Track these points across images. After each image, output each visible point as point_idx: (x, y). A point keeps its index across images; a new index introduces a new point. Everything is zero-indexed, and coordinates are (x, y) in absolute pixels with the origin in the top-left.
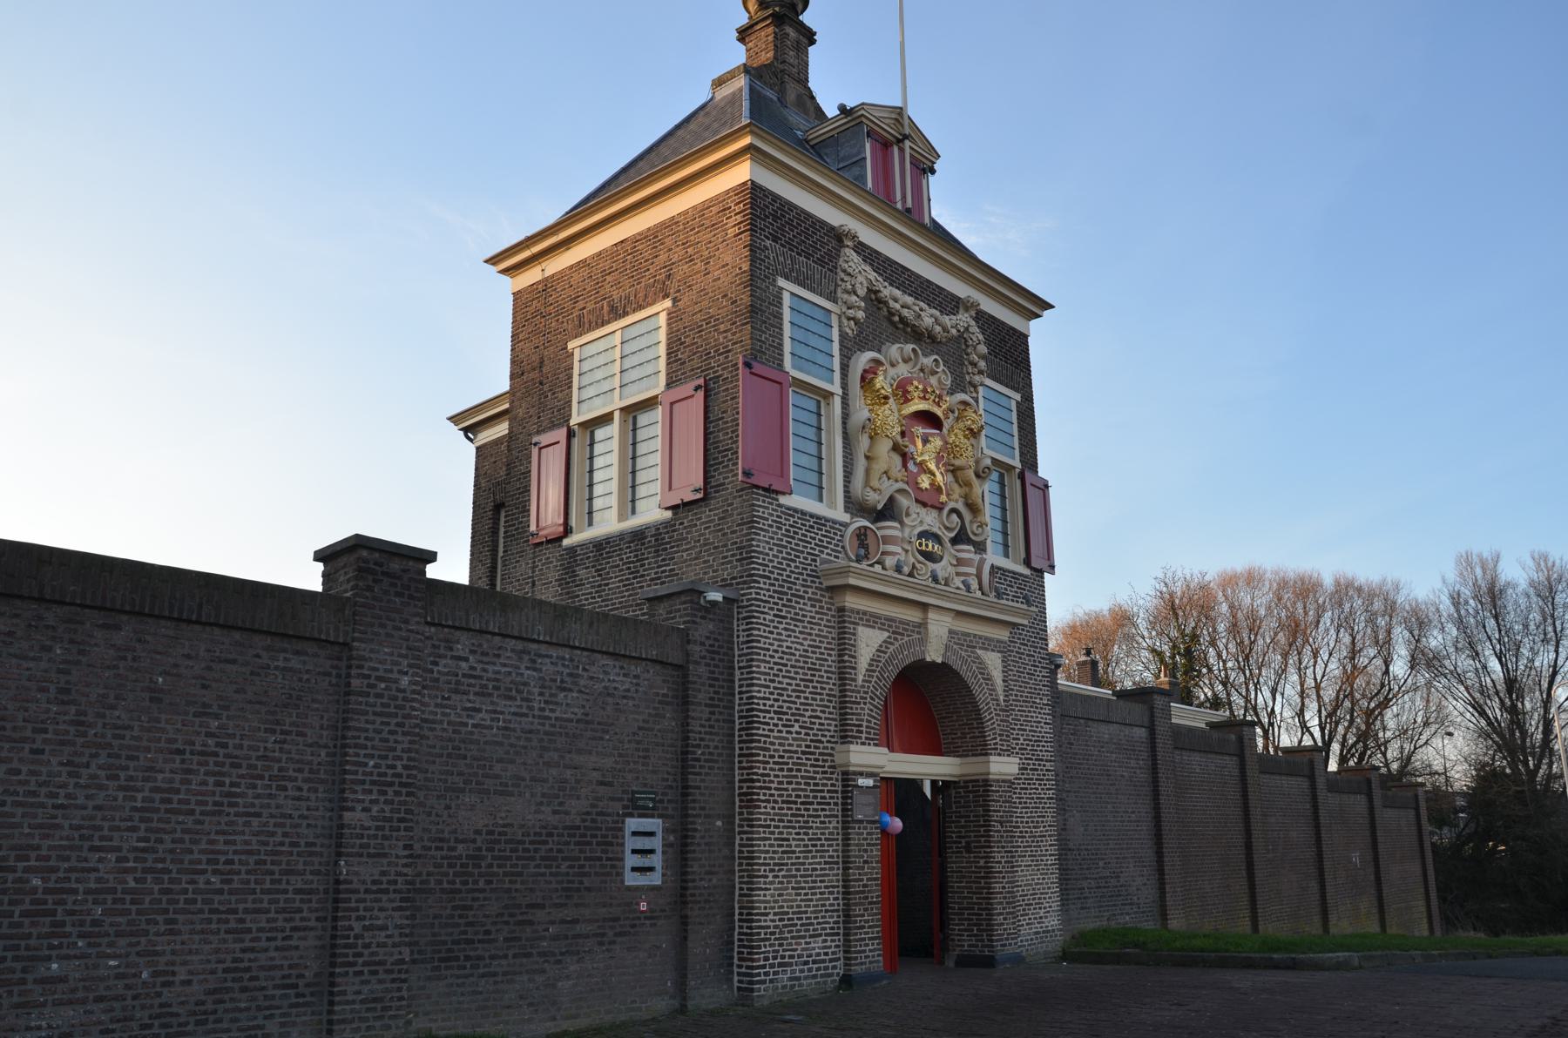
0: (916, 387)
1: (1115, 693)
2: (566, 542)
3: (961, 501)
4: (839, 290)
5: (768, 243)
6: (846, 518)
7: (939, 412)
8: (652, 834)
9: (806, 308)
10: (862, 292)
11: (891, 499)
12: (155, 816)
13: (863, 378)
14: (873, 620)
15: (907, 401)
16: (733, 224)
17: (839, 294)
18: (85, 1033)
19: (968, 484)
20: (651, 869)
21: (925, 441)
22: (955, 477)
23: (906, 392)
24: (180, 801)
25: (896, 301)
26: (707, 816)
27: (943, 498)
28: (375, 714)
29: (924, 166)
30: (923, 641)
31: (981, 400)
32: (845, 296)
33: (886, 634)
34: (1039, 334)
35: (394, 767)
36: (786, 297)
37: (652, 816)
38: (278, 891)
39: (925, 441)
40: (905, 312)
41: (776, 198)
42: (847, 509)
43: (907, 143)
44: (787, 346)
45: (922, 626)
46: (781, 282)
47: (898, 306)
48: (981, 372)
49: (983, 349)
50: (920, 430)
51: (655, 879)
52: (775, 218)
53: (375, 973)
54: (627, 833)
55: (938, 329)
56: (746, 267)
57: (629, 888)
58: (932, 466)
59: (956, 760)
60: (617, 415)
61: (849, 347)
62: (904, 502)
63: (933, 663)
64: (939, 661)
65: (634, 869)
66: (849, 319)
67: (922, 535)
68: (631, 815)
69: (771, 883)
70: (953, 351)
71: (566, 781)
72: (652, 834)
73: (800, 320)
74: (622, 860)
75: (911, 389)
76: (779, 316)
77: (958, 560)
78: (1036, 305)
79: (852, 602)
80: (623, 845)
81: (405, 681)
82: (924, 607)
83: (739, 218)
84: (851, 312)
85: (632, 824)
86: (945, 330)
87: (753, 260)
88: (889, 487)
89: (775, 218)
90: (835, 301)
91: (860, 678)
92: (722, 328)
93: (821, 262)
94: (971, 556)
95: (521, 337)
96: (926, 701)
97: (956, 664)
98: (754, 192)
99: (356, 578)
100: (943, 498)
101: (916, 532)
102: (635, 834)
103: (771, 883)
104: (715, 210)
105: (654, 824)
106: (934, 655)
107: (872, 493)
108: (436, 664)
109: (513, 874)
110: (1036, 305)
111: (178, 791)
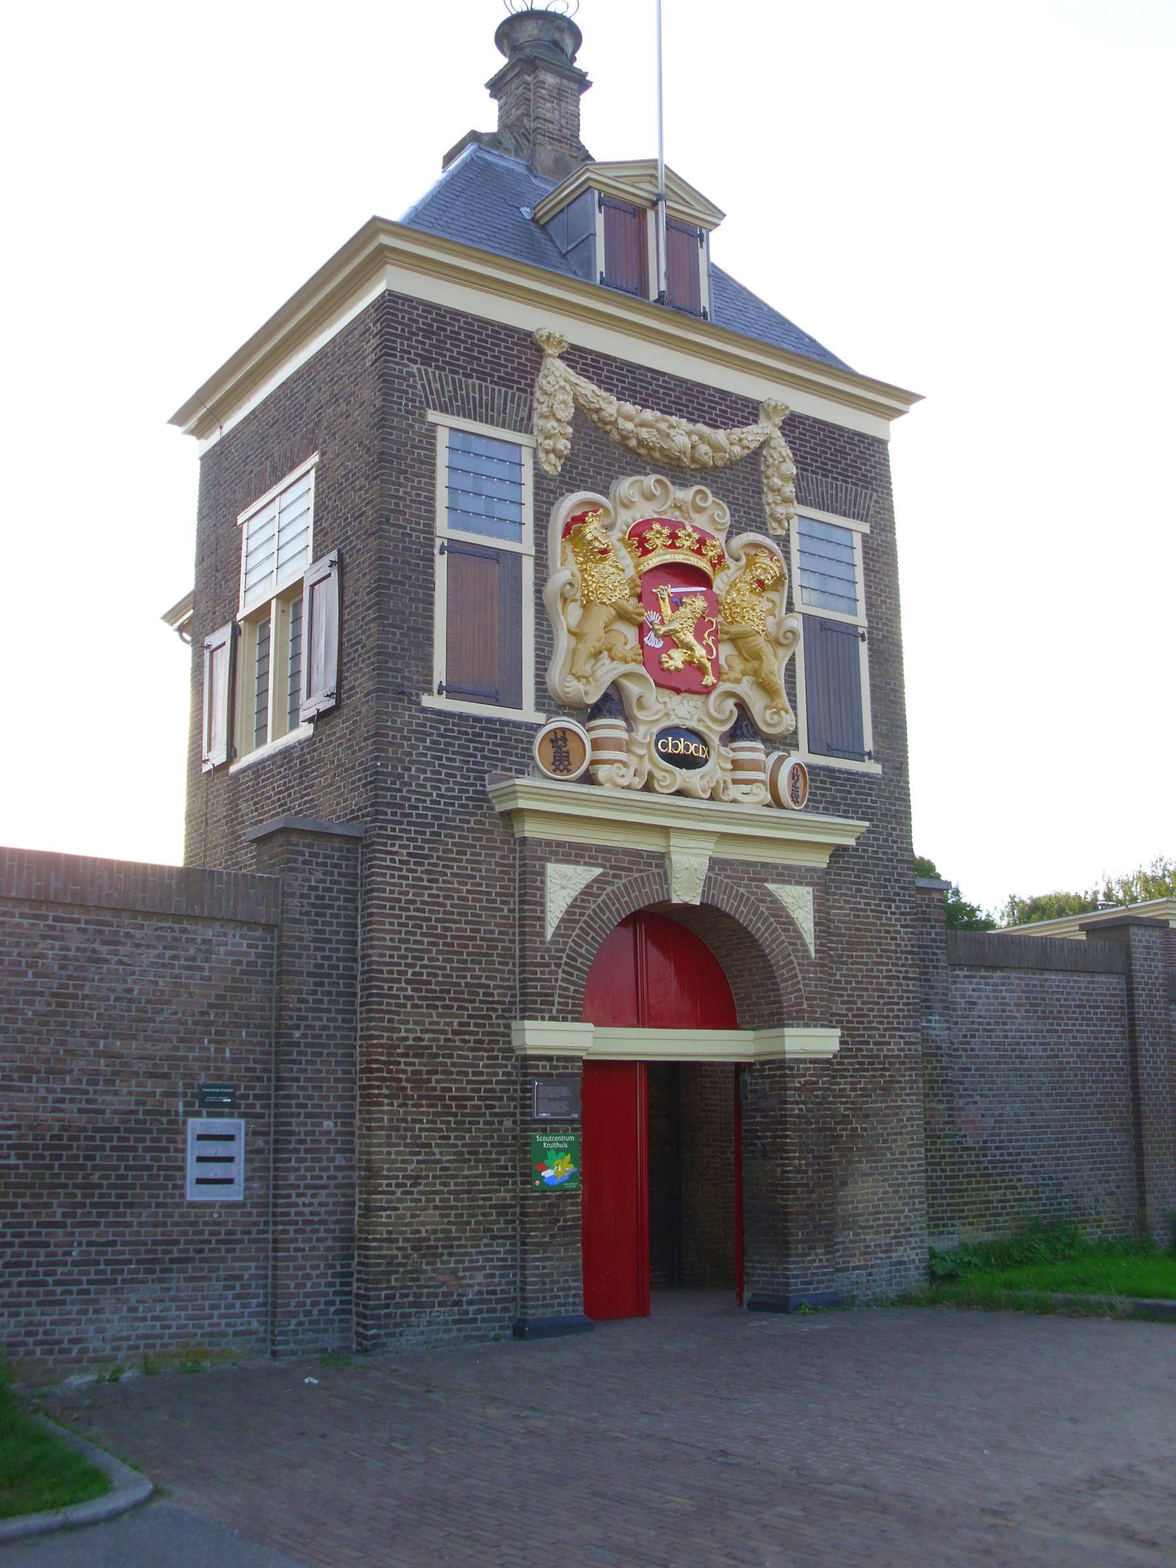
0: (657, 536)
1: (1088, 928)
3: (747, 681)
4: (535, 415)
5: (414, 368)
6: (540, 718)
7: (703, 564)
8: (231, 1138)
9: (819, 531)
10: (567, 413)
11: (615, 684)
13: (567, 530)
14: (574, 854)
15: (646, 552)
17: (536, 421)
19: (757, 656)
20: (201, 1137)
21: (677, 603)
22: (738, 648)
23: (642, 541)
25: (629, 418)
26: (309, 1115)
27: (709, 679)
29: (690, 229)
30: (664, 878)
31: (795, 543)
32: (541, 422)
33: (600, 870)
36: (443, 438)
37: (231, 1115)
39: (677, 603)
40: (644, 433)
42: (539, 706)
43: (661, 206)
44: (442, 498)
45: (661, 859)
46: (433, 416)
47: (630, 426)
48: (786, 501)
49: (791, 468)
50: (667, 591)
51: (235, 1193)
52: (428, 334)
53: (229, 1233)
54: (190, 1137)
55: (704, 449)
57: (192, 1205)
58: (690, 638)
59: (750, 1034)
61: (547, 492)
62: (633, 689)
63: (687, 907)
64: (697, 902)
65: (199, 1181)
66: (547, 452)
67: (664, 733)
68: (198, 1114)
69: (400, 1200)
70: (740, 484)
71: (97, 1072)
72: (231, 1138)
73: (812, 546)
74: (182, 1169)
75: (648, 535)
76: (431, 462)
77: (734, 762)
78: (893, 400)
79: (531, 830)
80: (184, 1151)
82: (665, 830)
84: (549, 444)
85: (196, 1125)
86: (716, 448)
88: (607, 672)
89: (428, 334)
90: (528, 430)
91: (550, 932)
93: (506, 382)
94: (760, 756)
96: (693, 953)
97: (725, 904)
100: (709, 679)
101: (655, 730)
102: (201, 1137)
103: (400, 1200)
105: (235, 1125)
106: (686, 890)
107: (575, 683)
109: (17, 1185)
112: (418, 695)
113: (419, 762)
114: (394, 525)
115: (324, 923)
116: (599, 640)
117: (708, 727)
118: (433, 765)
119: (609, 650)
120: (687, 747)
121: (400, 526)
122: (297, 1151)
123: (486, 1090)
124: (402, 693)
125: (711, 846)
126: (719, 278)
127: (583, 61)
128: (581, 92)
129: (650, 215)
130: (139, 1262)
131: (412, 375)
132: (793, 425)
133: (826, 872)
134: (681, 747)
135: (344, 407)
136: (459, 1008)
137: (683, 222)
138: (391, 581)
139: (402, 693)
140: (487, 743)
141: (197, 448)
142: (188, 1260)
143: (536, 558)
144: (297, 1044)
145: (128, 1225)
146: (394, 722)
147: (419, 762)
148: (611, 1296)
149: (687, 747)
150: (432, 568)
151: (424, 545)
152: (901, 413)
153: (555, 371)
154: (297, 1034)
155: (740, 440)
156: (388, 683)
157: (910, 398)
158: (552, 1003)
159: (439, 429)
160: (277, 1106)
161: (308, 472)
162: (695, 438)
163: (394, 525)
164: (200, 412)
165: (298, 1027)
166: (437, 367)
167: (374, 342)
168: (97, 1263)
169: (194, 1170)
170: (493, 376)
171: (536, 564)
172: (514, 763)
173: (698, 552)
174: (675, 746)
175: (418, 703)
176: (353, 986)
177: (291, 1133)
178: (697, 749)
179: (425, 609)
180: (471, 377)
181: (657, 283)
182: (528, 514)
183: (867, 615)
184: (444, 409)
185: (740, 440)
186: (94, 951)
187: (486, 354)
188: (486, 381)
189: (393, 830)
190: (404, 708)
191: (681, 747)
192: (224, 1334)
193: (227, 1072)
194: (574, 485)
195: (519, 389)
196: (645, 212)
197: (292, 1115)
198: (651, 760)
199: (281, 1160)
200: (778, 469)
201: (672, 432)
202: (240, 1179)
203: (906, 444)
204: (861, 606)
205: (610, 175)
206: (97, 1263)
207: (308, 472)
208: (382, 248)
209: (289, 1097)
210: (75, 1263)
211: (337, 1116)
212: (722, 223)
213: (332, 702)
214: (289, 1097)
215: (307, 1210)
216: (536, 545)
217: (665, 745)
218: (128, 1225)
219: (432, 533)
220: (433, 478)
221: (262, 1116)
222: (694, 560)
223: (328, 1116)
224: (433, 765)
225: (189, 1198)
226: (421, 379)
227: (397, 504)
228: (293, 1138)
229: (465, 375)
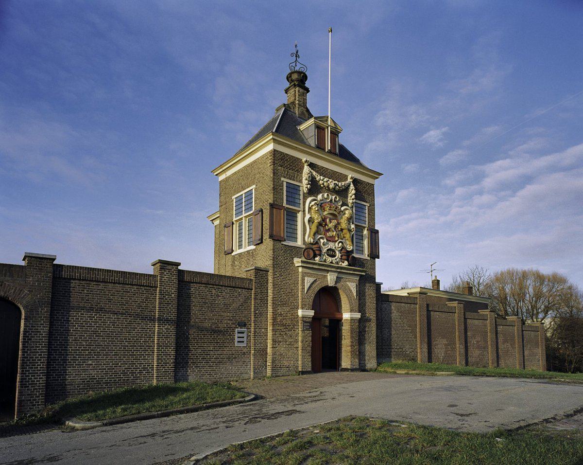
2: (233, 254)
12: (111, 329)
16: (269, 161)
18: (421, 464)
24: (117, 325)
28: (165, 303)
34: (377, 183)
35: (171, 316)
36: (285, 184)
38: (142, 346)
41: (282, 153)
46: (282, 179)
56: (272, 176)
60: (243, 218)
76: (282, 189)
81: (173, 295)
83: (270, 161)
87: (274, 174)
92: (266, 194)
95: (222, 195)
98: (275, 152)
99: (160, 270)
104: (265, 158)
108: (182, 291)
110: (377, 175)
111: (116, 323)
113: (60, 365)
125: (337, 274)
127: (307, 84)
128: (307, 93)
129: (326, 129)
130: (227, 358)
132: (355, 181)
133: (360, 319)
135: (262, 175)
142: (236, 358)
145: (225, 351)
147: (60, 365)
148: (315, 370)
152: (377, 178)
153: (306, 169)
157: (383, 174)
168: (219, 358)
169: (236, 339)
181: (328, 146)
182: (301, 202)
186: (218, 294)
192: (243, 373)
193: (243, 320)
202: (245, 342)
204: (367, 223)
206: (219, 358)
210: (215, 358)
213: (260, 242)
215: (259, 348)
218: (225, 351)
220: (283, 193)
222: (335, 212)
223: (263, 328)
225: (236, 345)
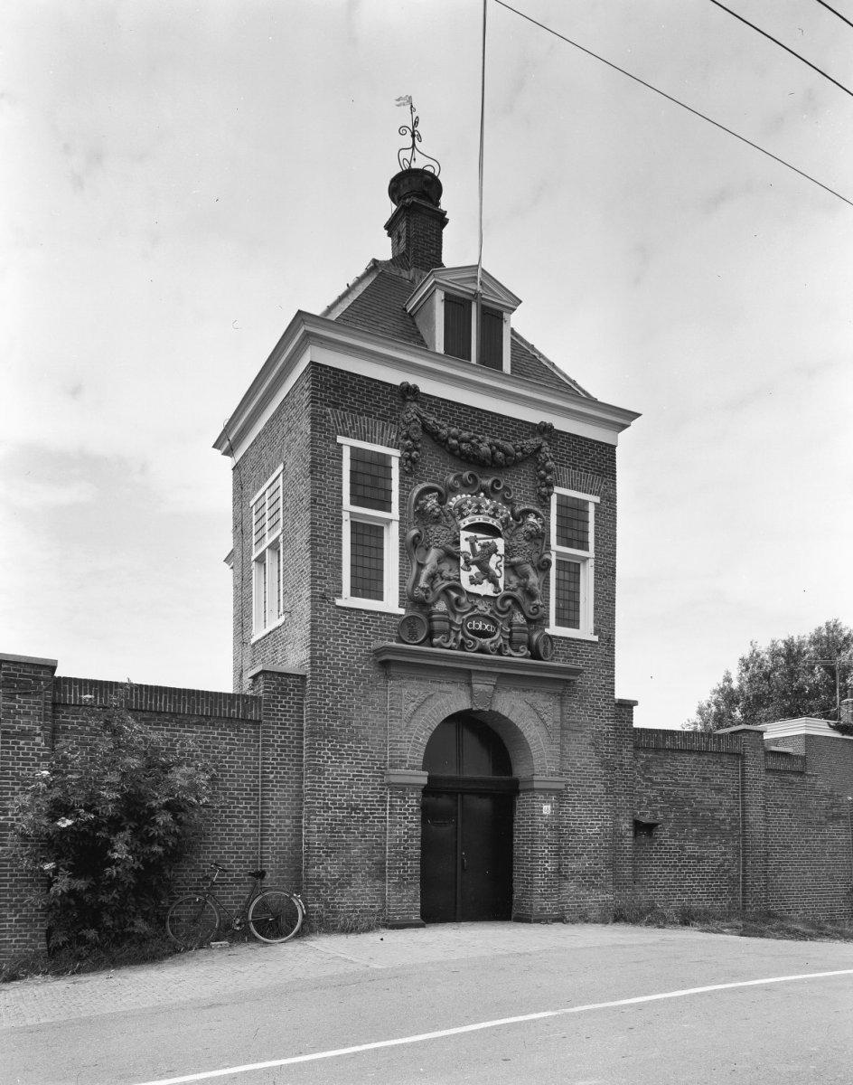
5: (329, 410)
25: (455, 437)
46: (340, 439)
112: (334, 599)
114: (318, 504)
115: (285, 720)
116: (434, 568)
117: (496, 615)
118: (342, 637)
119: (441, 573)
120: (483, 626)
121: (323, 505)
122: (271, 835)
123: (371, 805)
124: (325, 598)
126: (517, 340)
131: (326, 414)
134: (480, 626)
136: (357, 763)
137: (492, 309)
138: (318, 536)
139: (325, 598)
140: (372, 625)
141: (229, 462)
143: (400, 522)
144: (272, 782)
146: (321, 614)
149: (483, 626)
150: (341, 528)
151: (336, 515)
154: (272, 776)
155: (522, 448)
156: (318, 593)
158: (406, 761)
159: (344, 447)
160: (262, 812)
161: (279, 476)
162: (494, 448)
163: (318, 504)
164: (227, 442)
165: (272, 773)
166: (342, 409)
167: (307, 394)
170: (375, 414)
171: (400, 525)
172: (387, 636)
173: (494, 516)
174: (477, 626)
175: (334, 603)
176: (302, 717)
177: (269, 826)
178: (489, 628)
179: (337, 552)
180: (362, 415)
183: (595, 551)
184: (346, 435)
185: (522, 448)
187: (371, 400)
188: (371, 417)
189: (320, 704)
190: (326, 606)
191: (480, 626)
194: (423, 479)
195: (391, 422)
196: (470, 302)
197: (269, 817)
198: (464, 634)
199: (265, 821)
200: (544, 465)
201: (481, 445)
203: (626, 445)
205: (448, 279)
207: (279, 476)
208: (307, 335)
209: (267, 808)
211: (294, 818)
212: (518, 308)
214: (267, 808)
216: (400, 514)
217: (471, 626)
219: (340, 508)
221: (254, 817)
222: (491, 521)
224: (342, 637)
226: (333, 417)
227: (320, 492)
228: (270, 829)
229: (359, 414)
